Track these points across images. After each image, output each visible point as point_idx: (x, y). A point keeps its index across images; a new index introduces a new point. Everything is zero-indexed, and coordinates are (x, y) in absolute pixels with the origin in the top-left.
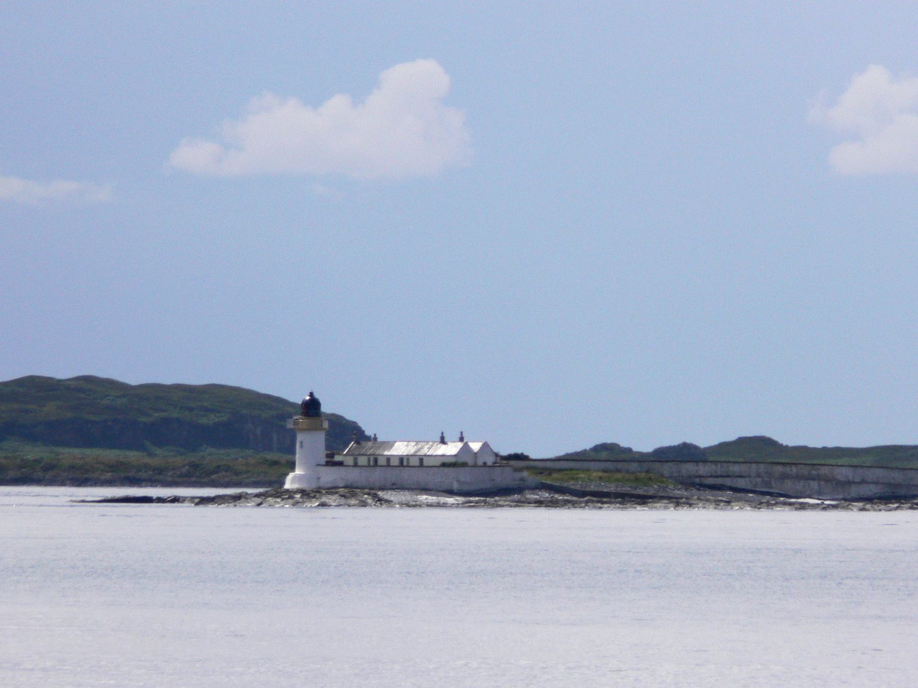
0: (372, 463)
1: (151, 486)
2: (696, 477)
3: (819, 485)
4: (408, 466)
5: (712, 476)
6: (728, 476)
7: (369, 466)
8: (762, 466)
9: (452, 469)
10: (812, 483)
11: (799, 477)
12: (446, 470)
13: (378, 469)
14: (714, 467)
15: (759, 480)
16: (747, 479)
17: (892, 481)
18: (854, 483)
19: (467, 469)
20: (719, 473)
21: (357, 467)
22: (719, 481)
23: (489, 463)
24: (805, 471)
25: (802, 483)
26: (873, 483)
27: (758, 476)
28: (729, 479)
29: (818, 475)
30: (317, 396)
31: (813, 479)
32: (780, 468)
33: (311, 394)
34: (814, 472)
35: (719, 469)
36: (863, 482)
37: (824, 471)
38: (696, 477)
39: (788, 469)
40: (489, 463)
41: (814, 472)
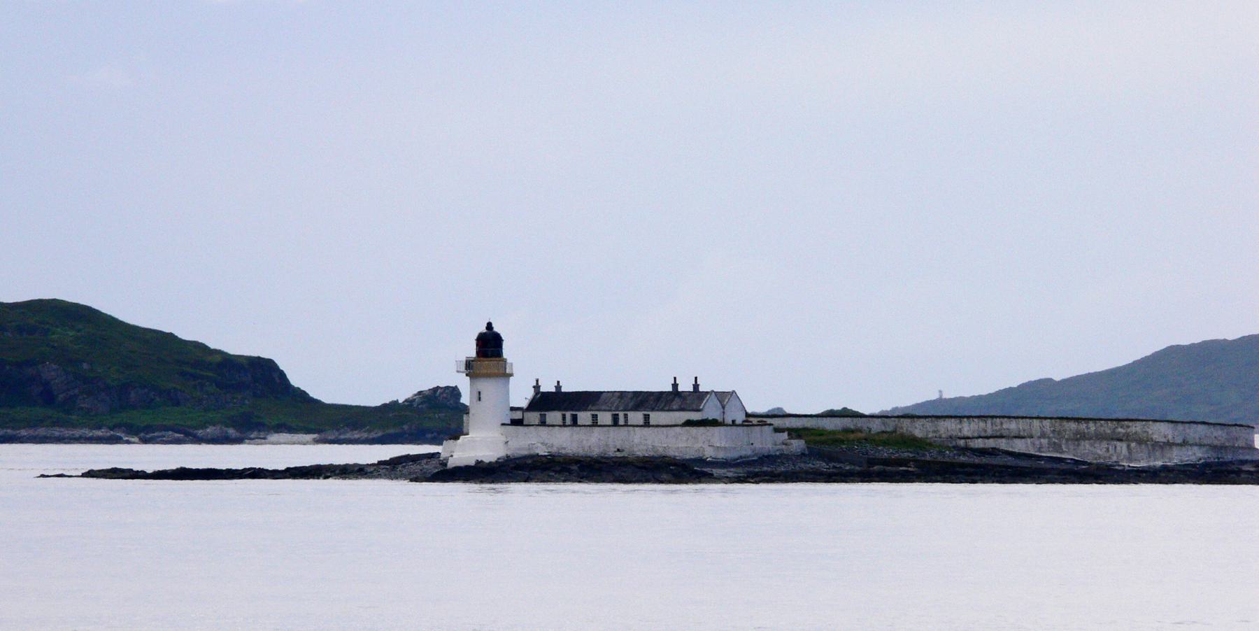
0: (568, 421)
1: (1081, 482)
2: (960, 438)
3: (1128, 446)
4: (626, 425)
5: (980, 437)
6: (1002, 437)
7: (564, 425)
8: (1047, 423)
9: (702, 429)
10: (1118, 444)
11: (1100, 437)
12: (694, 430)
13: (596, 429)
14: (982, 424)
15: (1044, 441)
16: (1029, 440)
17: (1216, 442)
18: (1174, 444)
19: (722, 428)
20: (989, 432)
21: (209, 398)
22: (991, 443)
23: (739, 421)
24: (1107, 428)
25: (1104, 444)
26: (1196, 445)
27: (1043, 435)
28: (1004, 440)
29: (1127, 435)
30: (496, 329)
31: (1121, 440)
32: (1073, 425)
33: (489, 326)
34: (1120, 430)
35: (989, 427)
36: (1185, 443)
37: (1136, 428)
38: (960, 438)
39: (1083, 426)
40: (739, 421)
41: (1120, 430)
